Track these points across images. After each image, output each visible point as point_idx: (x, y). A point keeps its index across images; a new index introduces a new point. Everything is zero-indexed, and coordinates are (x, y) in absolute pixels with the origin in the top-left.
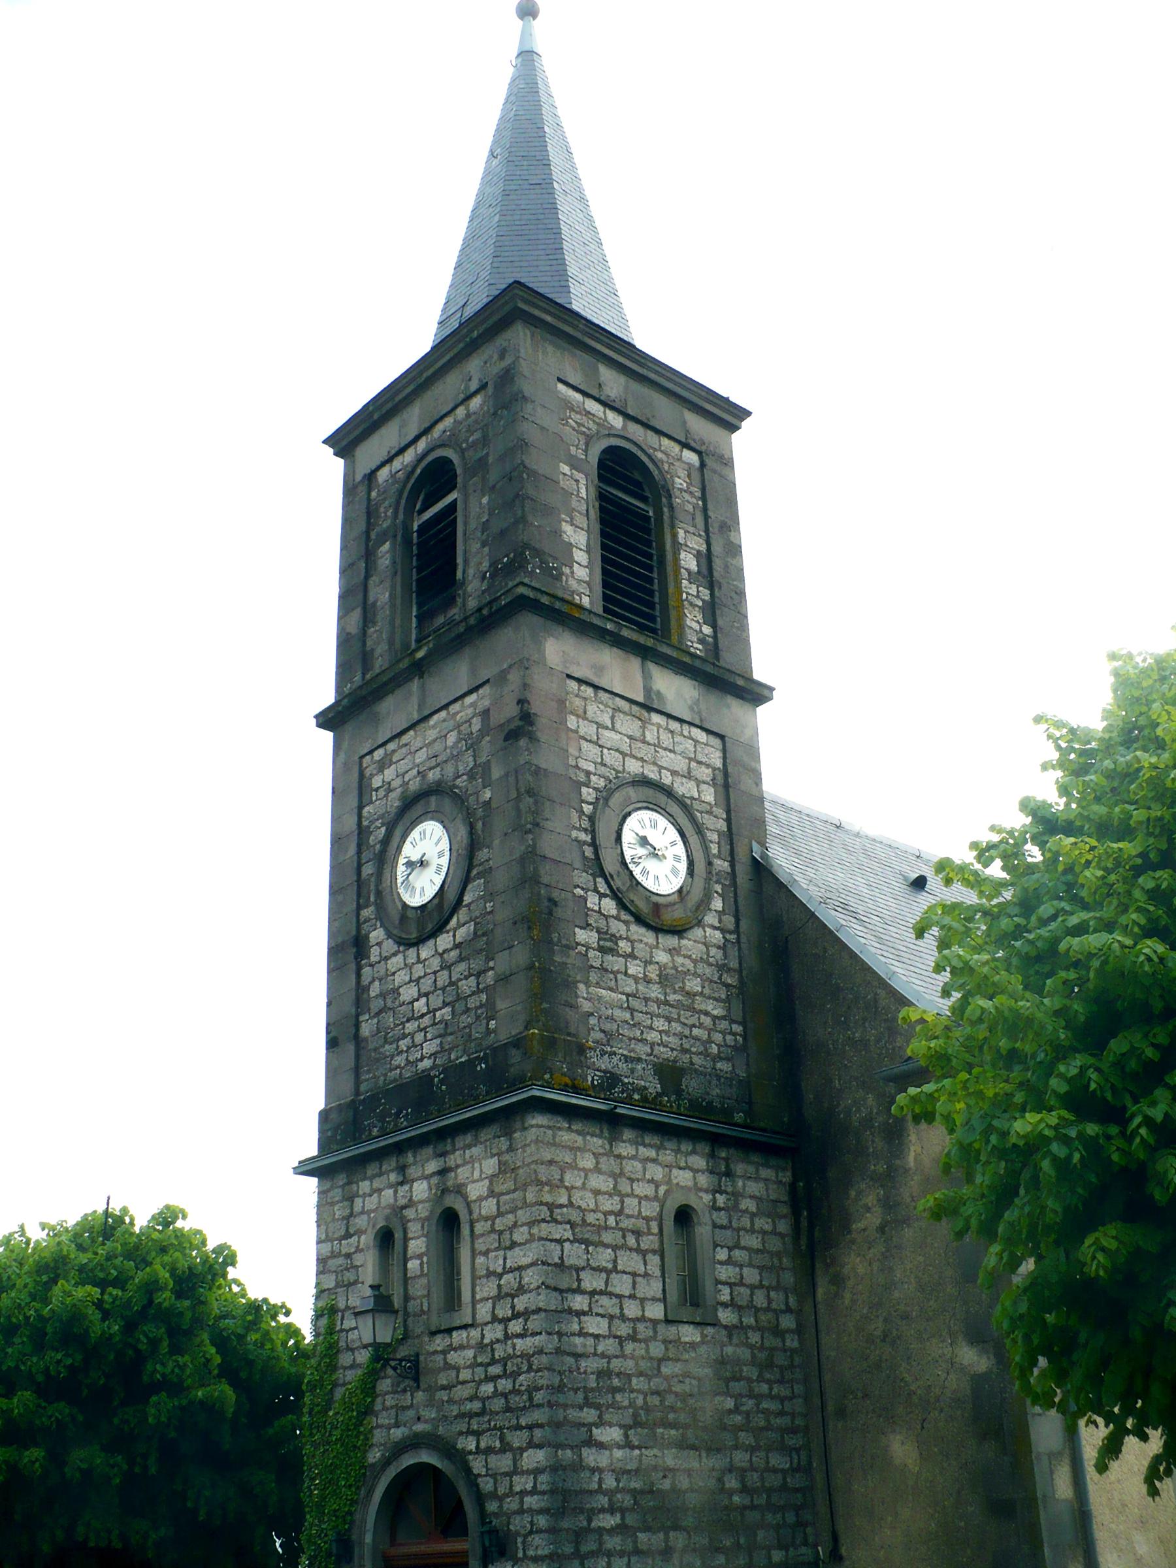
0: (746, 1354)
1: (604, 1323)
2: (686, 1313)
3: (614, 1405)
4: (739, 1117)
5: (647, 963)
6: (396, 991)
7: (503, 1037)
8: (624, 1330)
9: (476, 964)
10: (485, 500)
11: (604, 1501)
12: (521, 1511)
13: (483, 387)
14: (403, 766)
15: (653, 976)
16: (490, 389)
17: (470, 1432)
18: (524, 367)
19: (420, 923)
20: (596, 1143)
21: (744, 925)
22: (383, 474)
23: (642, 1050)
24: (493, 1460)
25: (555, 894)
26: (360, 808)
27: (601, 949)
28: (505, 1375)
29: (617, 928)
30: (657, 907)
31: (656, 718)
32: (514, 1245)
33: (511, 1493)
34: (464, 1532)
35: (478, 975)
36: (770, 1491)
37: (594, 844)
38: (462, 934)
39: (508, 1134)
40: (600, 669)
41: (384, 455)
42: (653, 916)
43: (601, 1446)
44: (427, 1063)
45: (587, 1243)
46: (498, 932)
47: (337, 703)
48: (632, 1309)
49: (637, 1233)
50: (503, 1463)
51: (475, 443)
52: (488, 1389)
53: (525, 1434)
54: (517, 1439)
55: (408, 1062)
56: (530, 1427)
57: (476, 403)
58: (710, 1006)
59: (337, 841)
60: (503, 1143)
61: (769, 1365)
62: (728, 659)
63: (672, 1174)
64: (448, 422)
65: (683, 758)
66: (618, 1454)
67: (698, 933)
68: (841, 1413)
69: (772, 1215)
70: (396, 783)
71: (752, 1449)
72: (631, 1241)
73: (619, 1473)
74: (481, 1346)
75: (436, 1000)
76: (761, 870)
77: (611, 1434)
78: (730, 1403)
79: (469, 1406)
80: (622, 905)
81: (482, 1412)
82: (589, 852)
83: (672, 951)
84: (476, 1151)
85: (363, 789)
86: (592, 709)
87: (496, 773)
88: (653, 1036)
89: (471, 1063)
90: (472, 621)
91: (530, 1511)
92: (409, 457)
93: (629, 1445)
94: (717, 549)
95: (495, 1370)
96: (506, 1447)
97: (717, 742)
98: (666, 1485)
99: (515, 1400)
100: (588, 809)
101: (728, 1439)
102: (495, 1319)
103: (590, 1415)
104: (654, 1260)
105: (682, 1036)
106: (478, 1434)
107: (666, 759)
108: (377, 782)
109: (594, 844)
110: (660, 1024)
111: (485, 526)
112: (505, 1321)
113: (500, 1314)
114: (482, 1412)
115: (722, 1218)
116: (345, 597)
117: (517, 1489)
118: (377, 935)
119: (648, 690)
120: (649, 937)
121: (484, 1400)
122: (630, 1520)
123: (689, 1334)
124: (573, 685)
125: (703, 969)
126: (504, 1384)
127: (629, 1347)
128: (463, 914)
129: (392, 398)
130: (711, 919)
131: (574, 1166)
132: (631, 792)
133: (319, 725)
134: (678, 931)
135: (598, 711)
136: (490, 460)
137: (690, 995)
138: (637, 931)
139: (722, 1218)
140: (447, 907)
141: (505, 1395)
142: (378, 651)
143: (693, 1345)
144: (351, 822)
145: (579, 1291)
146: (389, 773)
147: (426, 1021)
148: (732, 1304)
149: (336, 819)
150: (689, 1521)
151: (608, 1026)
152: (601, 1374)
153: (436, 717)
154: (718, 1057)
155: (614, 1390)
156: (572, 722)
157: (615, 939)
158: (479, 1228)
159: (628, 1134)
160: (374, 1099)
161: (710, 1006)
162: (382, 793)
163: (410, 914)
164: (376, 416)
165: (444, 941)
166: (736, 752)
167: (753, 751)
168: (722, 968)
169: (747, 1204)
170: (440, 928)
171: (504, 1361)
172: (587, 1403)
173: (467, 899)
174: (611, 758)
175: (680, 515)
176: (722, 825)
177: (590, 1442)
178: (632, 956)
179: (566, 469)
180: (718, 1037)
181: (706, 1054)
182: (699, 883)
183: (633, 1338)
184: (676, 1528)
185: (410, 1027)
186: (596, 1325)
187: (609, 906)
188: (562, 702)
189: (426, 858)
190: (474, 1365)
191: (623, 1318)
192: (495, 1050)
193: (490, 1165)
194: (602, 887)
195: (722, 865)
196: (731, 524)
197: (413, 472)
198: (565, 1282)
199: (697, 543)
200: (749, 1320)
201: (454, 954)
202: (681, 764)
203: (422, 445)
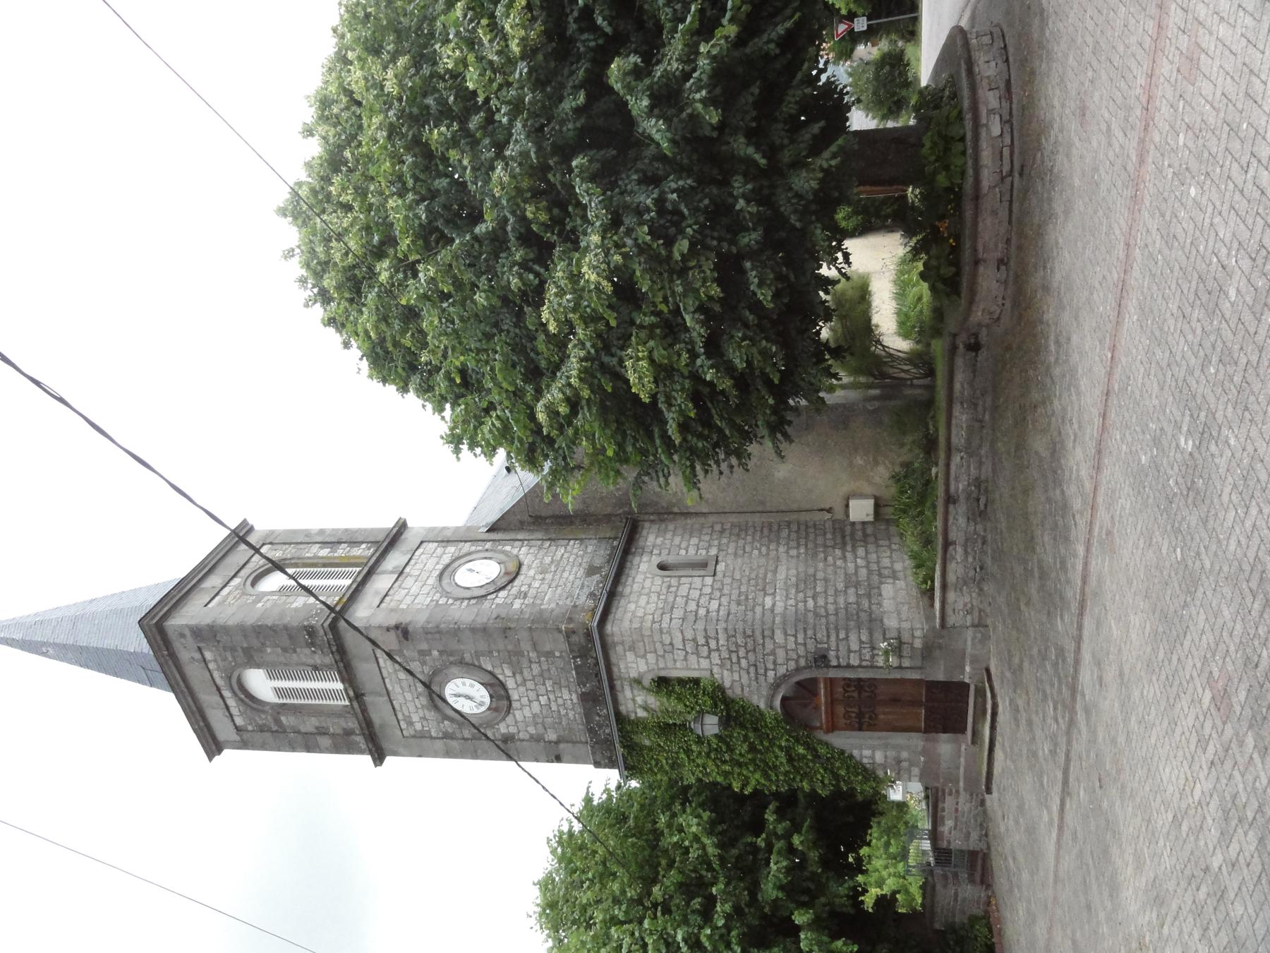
0: (732, 545)
1: (713, 602)
2: (711, 568)
3: (754, 599)
4: (615, 543)
5: (534, 578)
6: (535, 716)
7: (565, 647)
8: (717, 594)
9: (525, 664)
10: (269, 650)
11: (801, 605)
12: (805, 644)
13: (200, 649)
14: (412, 709)
15: (541, 576)
16: (201, 645)
17: (765, 675)
18: (193, 622)
19: (499, 698)
20: (623, 602)
21: (519, 537)
22: (239, 721)
23: (578, 583)
24: (780, 661)
25: (494, 616)
26: (431, 738)
27: (525, 598)
28: (737, 652)
29: (514, 591)
30: (507, 573)
31: (407, 570)
32: (671, 644)
33: (795, 650)
34: (814, 681)
35: (531, 662)
36: (798, 538)
37: (469, 599)
38: (508, 672)
39: (615, 644)
40: (377, 593)
41: (228, 720)
42: (512, 576)
43: (774, 605)
44: (574, 697)
45: (673, 607)
46: (510, 647)
47: (371, 753)
48: (707, 590)
49: (669, 587)
50: (781, 654)
51: (234, 658)
52: (744, 662)
53: (767, 641)
54: (769, 646)
55: (573, 709)
56: (764, 637)
57: (208, 655)
58: (559, 554)
59: (449, 754)
60: (619, 649)
61: (738, 535)
62: (380, 537)
63: (643, 572)
64: (216, 675)
65: (430, 561)
66: (778, 598)
67: (521, 557)
68: (762, 503)
69: (666, 531)
70: (421, 713)
71: (778, 543)
72: (673, 589)
73: (787, 597)
74: (722, 666)
75: (542, 690)
76: (493, 528)
77: (768, 601)
78: (756, 552)
79: (752, 675)
80: (503, 588)
81: (755, 665)
82: (473, 601)
83: (529, 567)
84: (622, 666)
85: (422, 735)
86: (397, 597)
87: (424, 646)
88: (571, 578)
89: (577, 668)
90: (338, 658)
91: (805, 639)
92: (232, 703)
93: (774, 594)
94: (320, 539)
95: (734, 659)
96: (773, 653)
97: (424, 545)
98: (794, 579)
99: (750, 646)
100: (451, 601)
101: (773, 554)
102: (708, 657)
103: (758, 610)
104: (683, 580)
105: (573, 566)
106: (766, 670)
107: (429, 566)
108: (418, 726)
109: (469, 599)
110: (566, 575)
111: (285, 650)
112: (710, 651)
113: (705, 654)
114: (755, 665)
115: (665, 552)
116: (309, 748)
117: (793, 646)
118: (503, 728)
119: (392, 572)
120: (521, 578)
121: (749, 666)
122: (810, 593)
123: (721, 567)
124: (383, 605)
125: (540, 556)
126: (742, 653)
127: (726, 591)
128: (497, 671)
129: (193, 713)
130: (515, 551)
131: (634, 613)
132: (445, 581)
133: (381, 763)
134: (520, 565)
135: (398, 595)
136: (245, 645)
137: (552, 562)
138: (516, 583)
139: (665, 552)
140: (493, 681)
141: (747, 652)
142: (344, 725)
143: (727, 566)
144: (439, 744)
145: (696, 612)
146: (415, 718)
147: (552, 697)
148: (707, 549)
149: (435, 754)
150: (811, 571)
151: (565, 595)
152: (739, 604)
153: (389, 686)
154: (585, 552)
155: (747, 599)
156: (403, 606)
157: (520, 592)
158: (662, 665)
159: (620, 589)
160: (591, 731)
161: (559, 554)
162: (425, 723)
163: (494, 706)
164: (202, 724)
165: (510, 684)
166: (430, 537)
167: (432, 529)
168: (540, 548)
169: (659, 541)
170: (503, 685)
171: (731, 652)
172: (753, 610)
173: (490, 668)
174: (426, 589)
175: (296, 555)
176: (468, 544)
177: (772, 610)
178: (530, 586)
179: (260, 605)
180: (575, 551)
181: (582, 557)
182: (496, 555)
183: (721, 590)
184: (814, 576)
185: (554, 708)
186: (714, 605)
187: (503, 594)
188: (392, 610)
189: (466, 694)
190: (731, 670)
191: (711, 593)
192: (572, 651)
193: (630, 656)
194: (493, 596)
195: (488, 545)
196: (307, 533)
197: (242, 700)
198: (692, 618)
199: (315, 548)
200: (716, 543)
201: (518, 677)
202: (434, 560)
203: (227, 694)
